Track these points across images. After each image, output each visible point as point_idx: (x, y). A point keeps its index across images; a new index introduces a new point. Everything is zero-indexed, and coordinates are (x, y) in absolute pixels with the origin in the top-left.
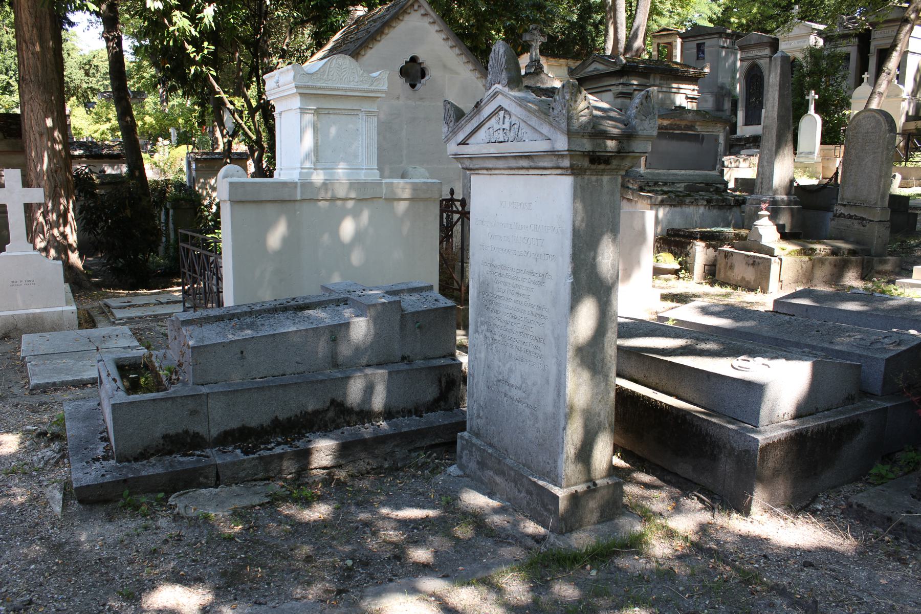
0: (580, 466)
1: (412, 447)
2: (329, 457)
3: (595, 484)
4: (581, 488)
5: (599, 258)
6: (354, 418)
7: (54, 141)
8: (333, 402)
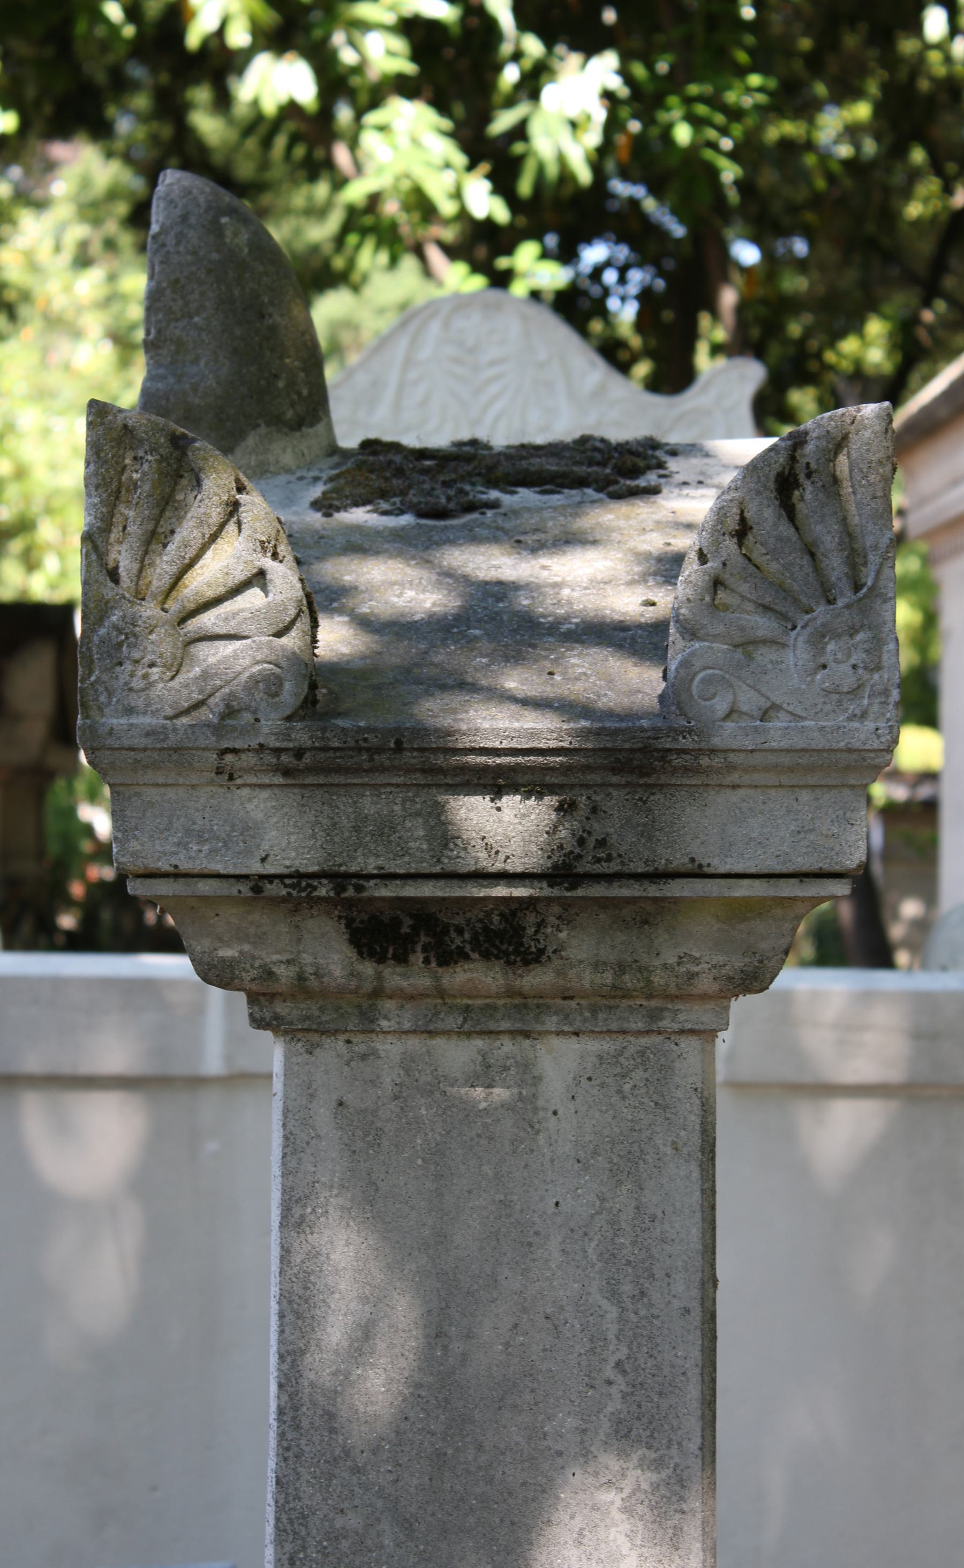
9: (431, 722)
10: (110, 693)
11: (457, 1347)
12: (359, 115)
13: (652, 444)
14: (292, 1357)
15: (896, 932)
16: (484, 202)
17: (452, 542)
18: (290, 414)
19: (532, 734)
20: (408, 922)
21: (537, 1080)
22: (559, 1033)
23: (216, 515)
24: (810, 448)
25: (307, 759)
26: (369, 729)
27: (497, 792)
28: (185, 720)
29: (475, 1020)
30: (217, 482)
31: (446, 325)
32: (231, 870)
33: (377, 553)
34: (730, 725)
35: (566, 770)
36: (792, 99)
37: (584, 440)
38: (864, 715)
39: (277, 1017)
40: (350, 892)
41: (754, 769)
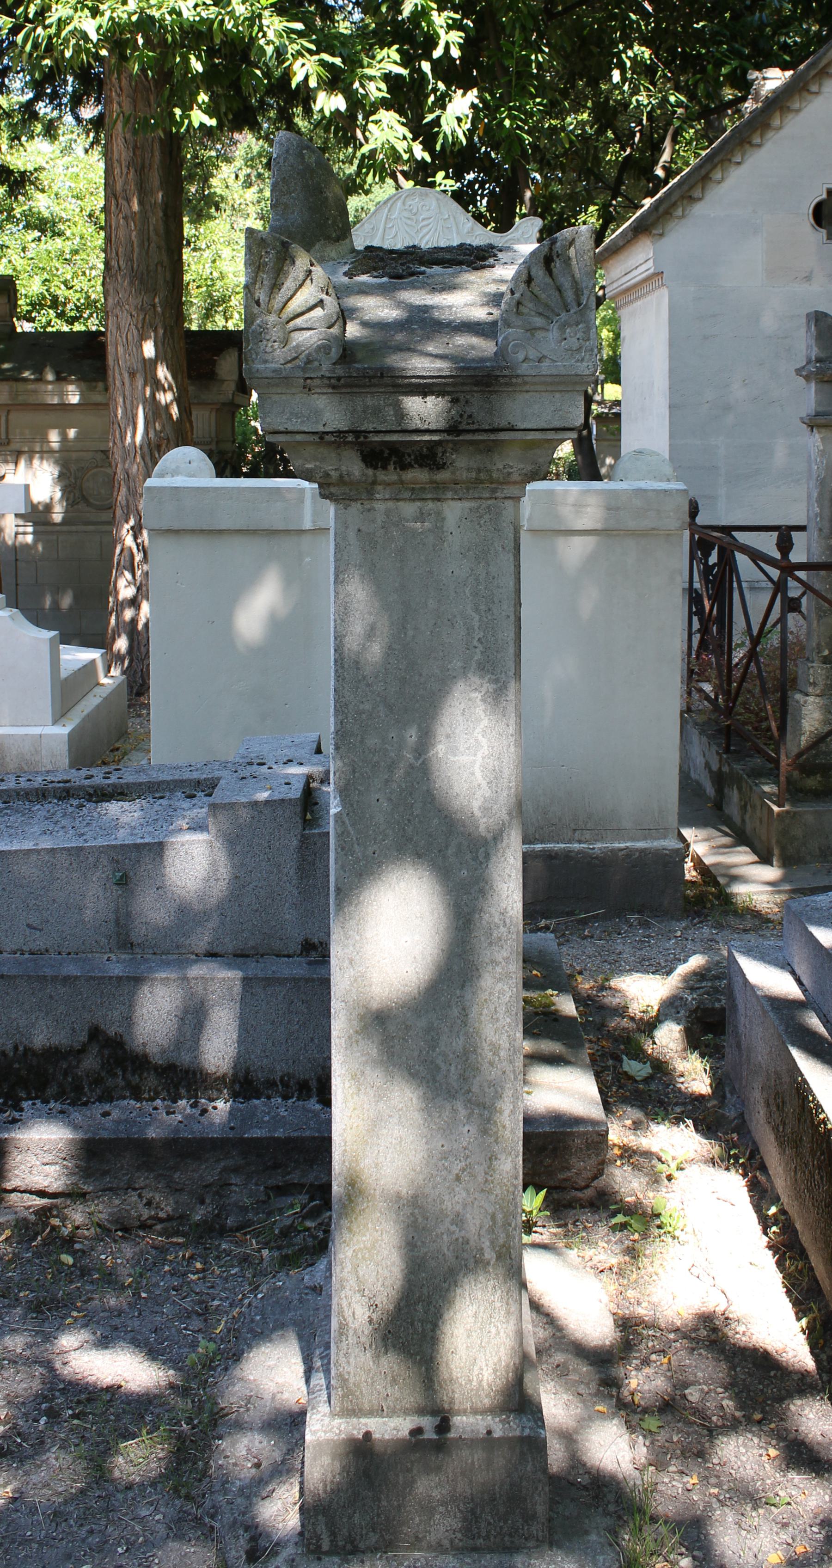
0: (390, 1362)
1: (277, 1180)
2: (53, 1170)
3: (444, 1426)
4: (389, 1428)
5: (440, 749)
6: (151, 1081)
7: (157, 385)
8: (95, 1033)
9: (395, 365)
10: (257, 354)
11: (410, 633)
12: (366, 118)
13: (492, 247)
14: (339, 638)
15: (603, 471)
16: (420, 153)
17: (405, 289)
18: (334, 235)
19: (440, 370)
20: (387, 451)
21: (444, 519)
22: (453, 499)
23: (301, 276)
24: (558, 244)
25: (342, 381)
26: (369, 368)
27: (425, 395)
28: (289, 365)
29: (417, 494)
30: (302, 261)
31: (404, 203)
32: (310, 430)
33: (372, 294)
34: (525, 365)
35: (454, 385)
36: (553, 109)
37: (462, 245)
38: (582, 360)
39: (331, 494)
40: (362, 439)
41: (535, 384)
